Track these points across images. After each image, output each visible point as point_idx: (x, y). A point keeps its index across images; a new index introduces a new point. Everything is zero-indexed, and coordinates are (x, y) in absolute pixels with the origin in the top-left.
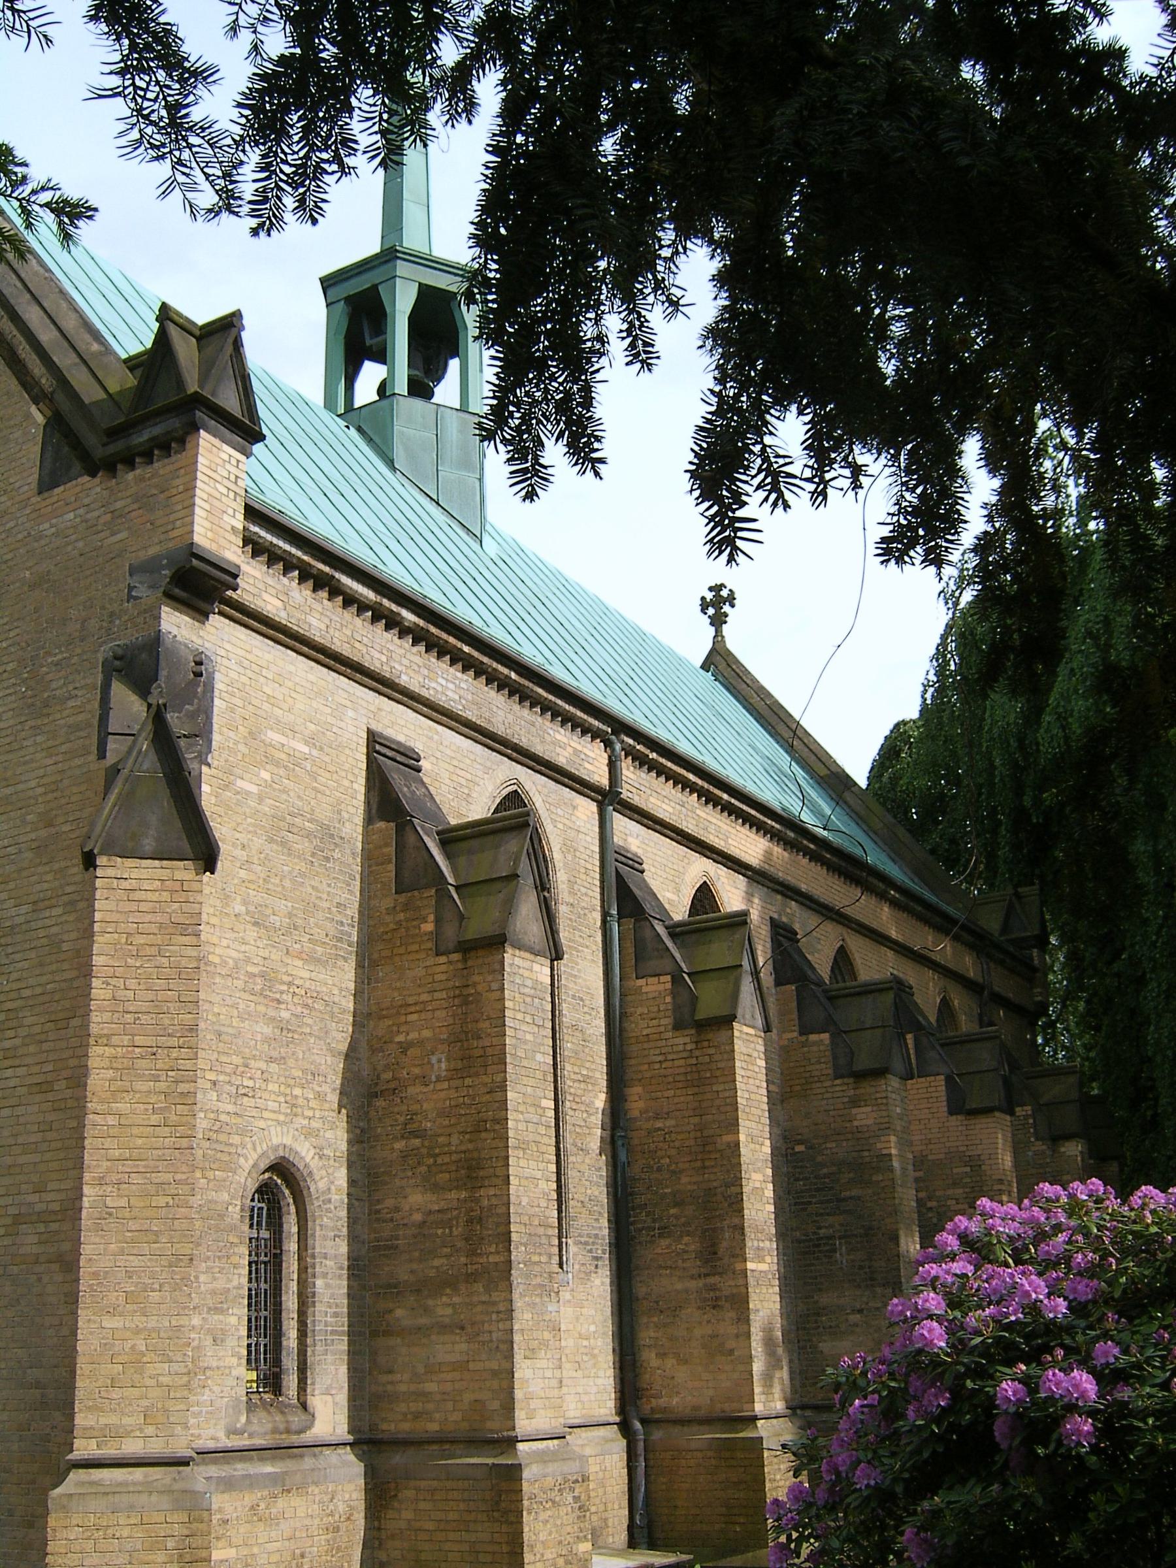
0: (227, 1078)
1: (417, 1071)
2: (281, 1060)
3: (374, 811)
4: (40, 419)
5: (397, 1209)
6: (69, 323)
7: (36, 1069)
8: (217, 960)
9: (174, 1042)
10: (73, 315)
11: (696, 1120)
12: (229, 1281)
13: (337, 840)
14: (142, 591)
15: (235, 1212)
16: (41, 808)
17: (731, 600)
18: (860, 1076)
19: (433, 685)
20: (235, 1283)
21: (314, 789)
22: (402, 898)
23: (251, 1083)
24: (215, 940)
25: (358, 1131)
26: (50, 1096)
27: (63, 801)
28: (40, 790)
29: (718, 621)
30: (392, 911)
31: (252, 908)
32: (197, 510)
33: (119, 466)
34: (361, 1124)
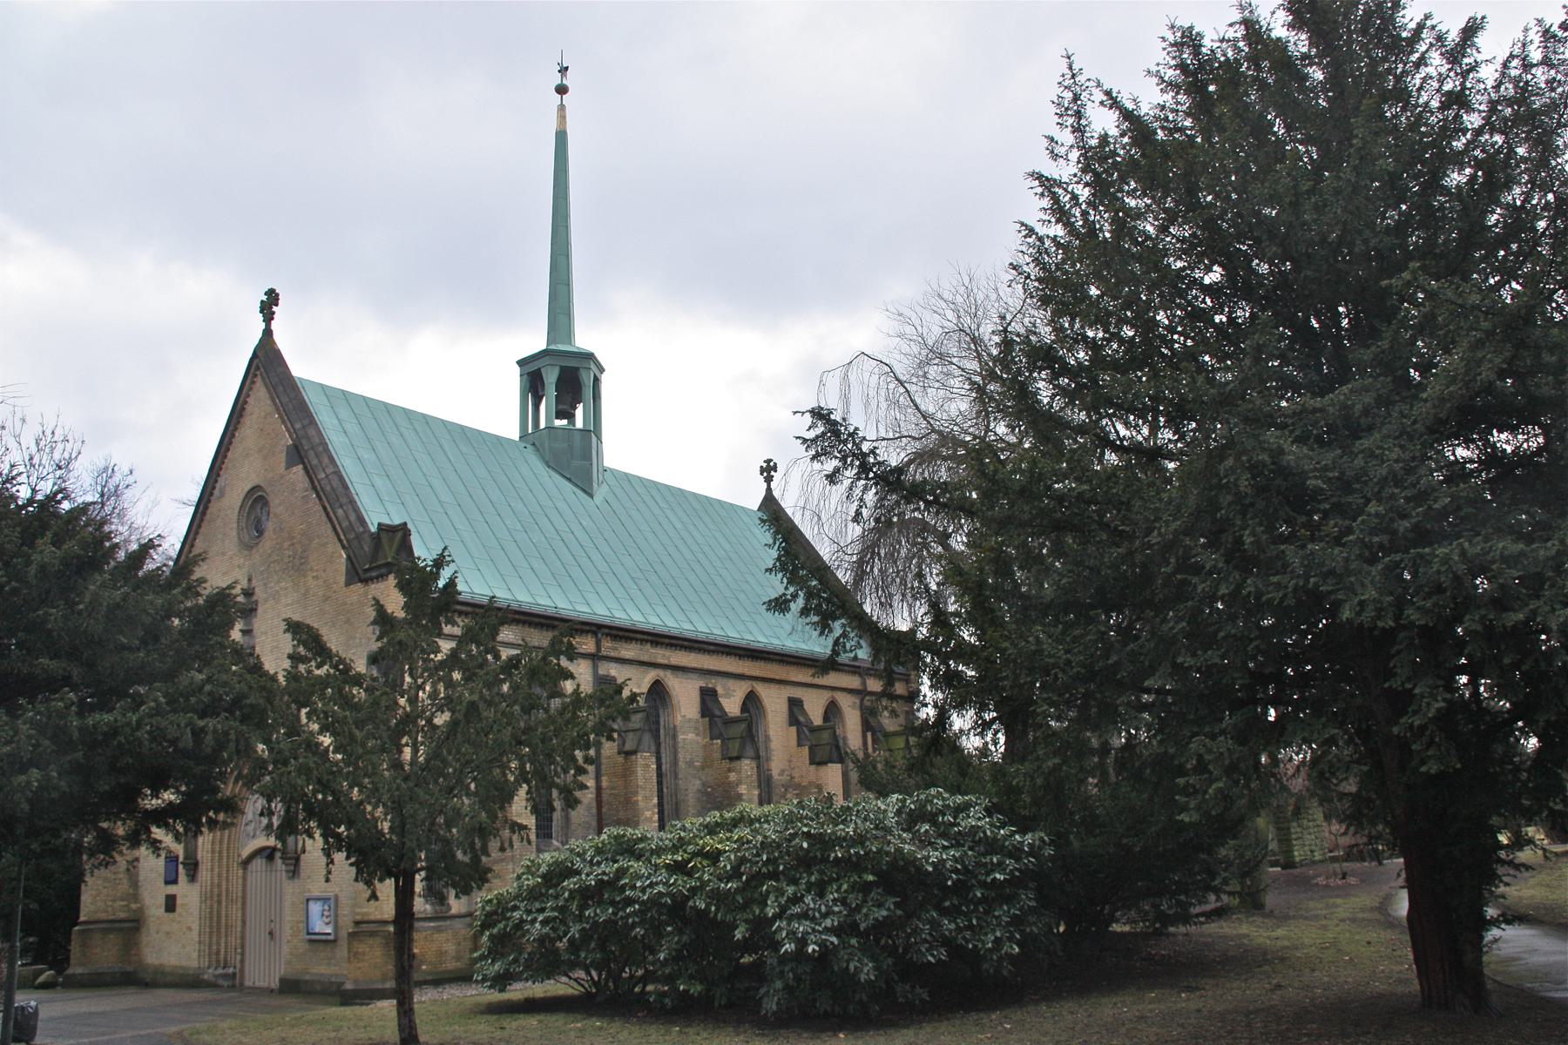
17: (775, 468)
18: (731, 759)
29: (769, 480)
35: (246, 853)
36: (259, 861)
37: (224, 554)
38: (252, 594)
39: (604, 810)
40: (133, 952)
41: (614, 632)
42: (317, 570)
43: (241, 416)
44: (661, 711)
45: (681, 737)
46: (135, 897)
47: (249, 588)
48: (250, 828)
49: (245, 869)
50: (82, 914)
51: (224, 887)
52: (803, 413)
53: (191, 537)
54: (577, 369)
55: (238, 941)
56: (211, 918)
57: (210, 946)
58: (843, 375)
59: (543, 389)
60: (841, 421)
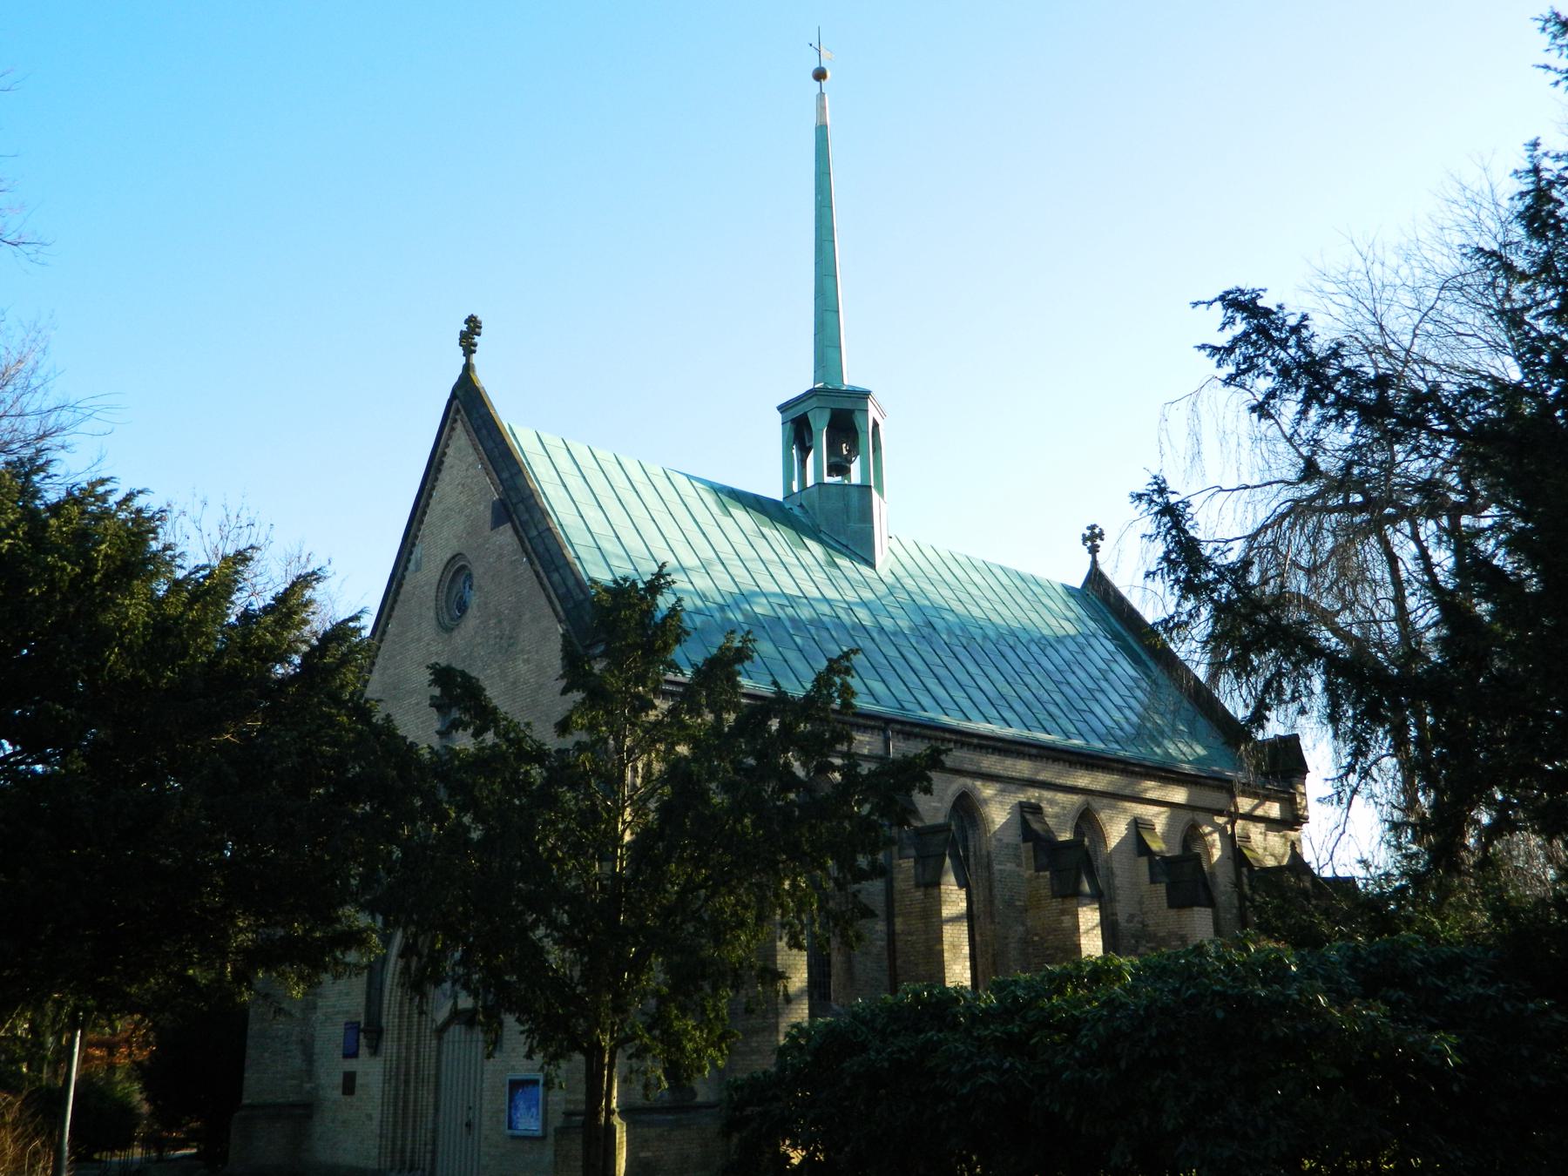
11: (924, 937)
17: (1101, 535)
29: (1094, 550)
39: (899, 962)
41: (907, 728)
42: (529, 652)
43: (439, 470)
44: (970, 832)
45: (997, 867)
46: (310, 1073)
49: (440, 1039)
50: (245, 1095)
51: (413, 1063)
52: (1210, 303)
53: (383, 621)
54: (851, 412)
56: (396, 1105)
57: (394, 1144)
58: (1190, 407)
59: (811, 439)
60: (1275, 309)
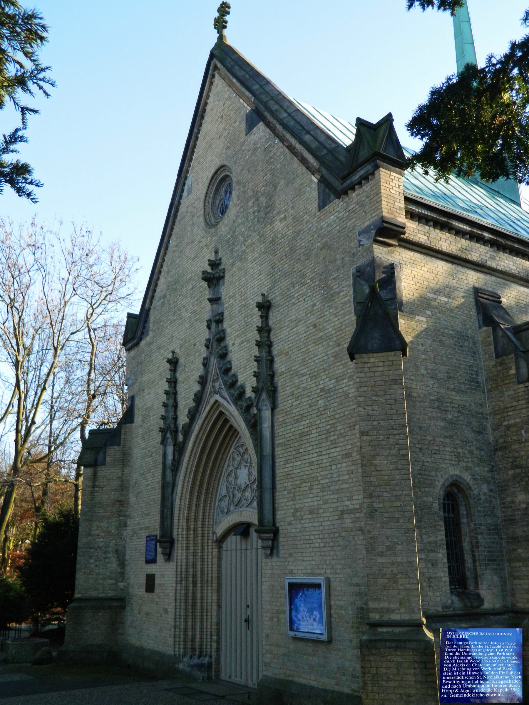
0: (426, 447)
1: (515, 438)
2: (451, 437)
3: (481, 323)
4: (316, 180)
5: (513, 502)
6: (322, 138)
7: (344, 448)
8: (416, 395)
9: (396, 432)
10: (323, 135)
12: (436, 537)
13: (466, 338)
14: (365, 241)
15: (436, 506)
16: (335, 339)
19: (503, 264)
20: (439, 538)
21: (452, 316)
22: (499, 360)
23: (437, 448)
24: (414, 386)
25: (490, 467)
26: (351, 459)
27: (343, 335)
28: (334, 332)
30: (495, 366)
31: (429, 371)
32: (383, 202)
33: (349, 192)
34: (492, 463)
35: (220, 530)
36: (234, 537)
37: (192, 242)
38: (219, 264)
40: (120, 631)
46: (122, 575)
47: (217, 260)
48: (224, 504)
49: (220, 548)
51: (199, 567)
55: (214, 627)
57: (185, 631)
